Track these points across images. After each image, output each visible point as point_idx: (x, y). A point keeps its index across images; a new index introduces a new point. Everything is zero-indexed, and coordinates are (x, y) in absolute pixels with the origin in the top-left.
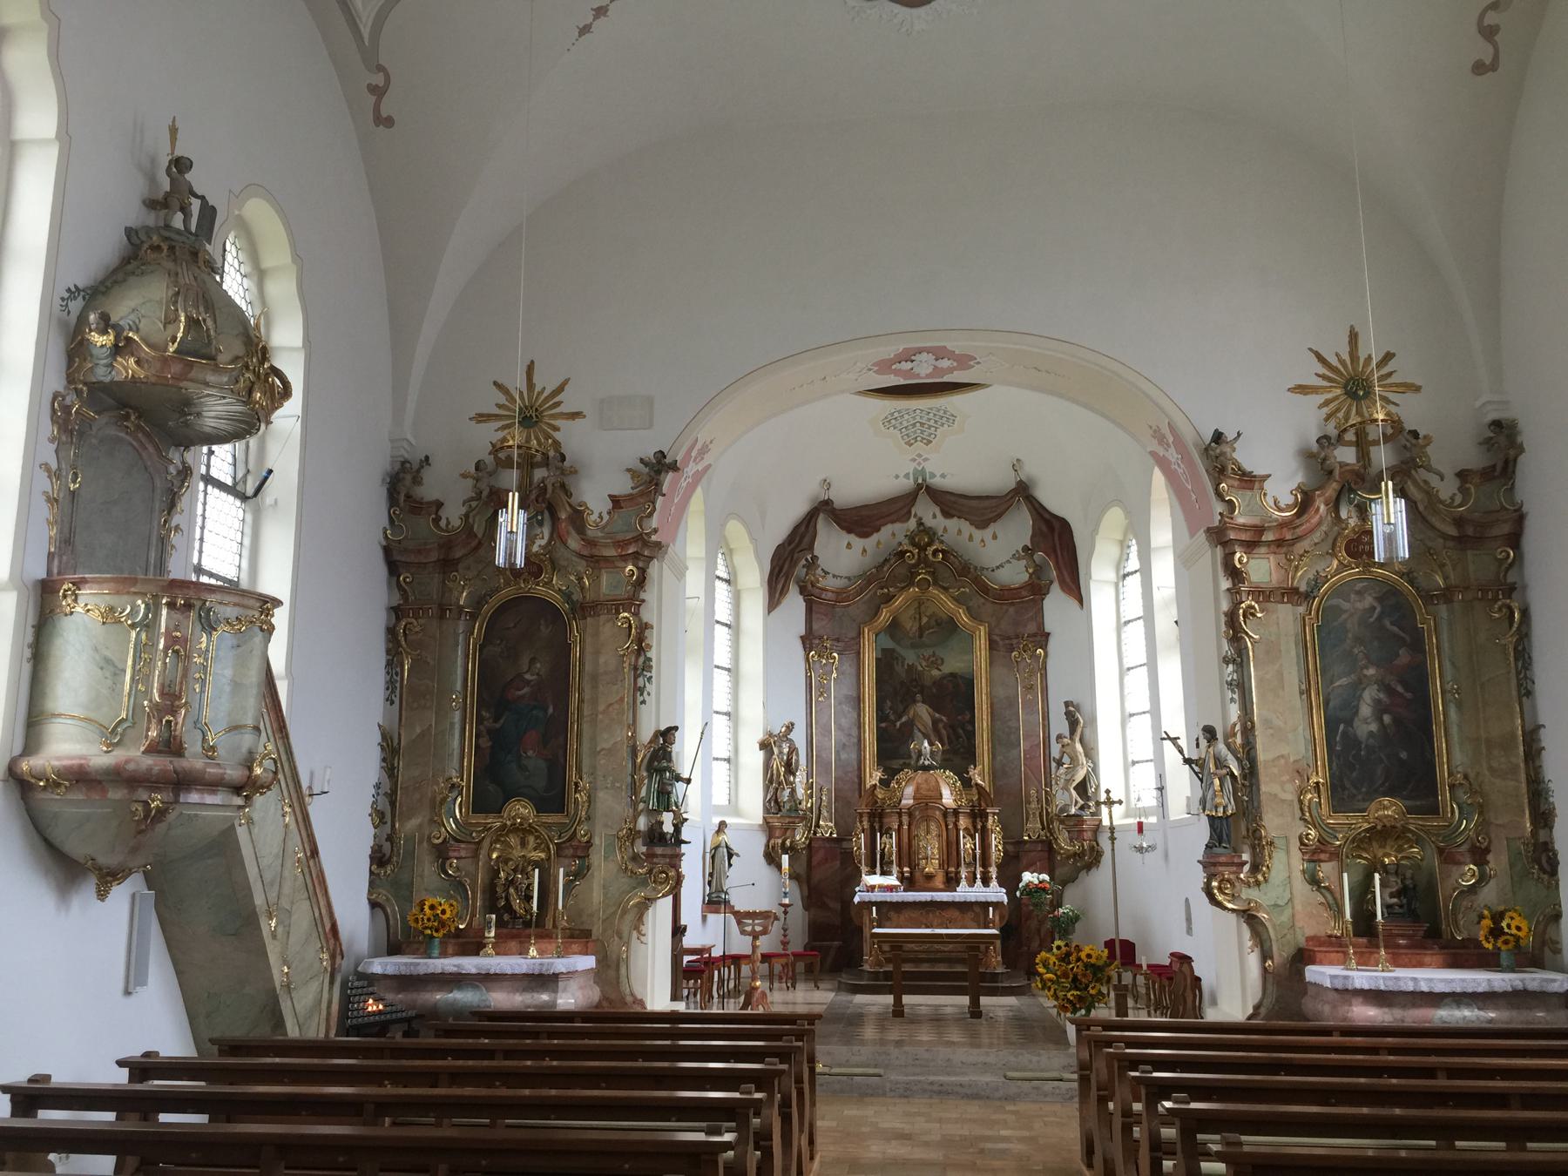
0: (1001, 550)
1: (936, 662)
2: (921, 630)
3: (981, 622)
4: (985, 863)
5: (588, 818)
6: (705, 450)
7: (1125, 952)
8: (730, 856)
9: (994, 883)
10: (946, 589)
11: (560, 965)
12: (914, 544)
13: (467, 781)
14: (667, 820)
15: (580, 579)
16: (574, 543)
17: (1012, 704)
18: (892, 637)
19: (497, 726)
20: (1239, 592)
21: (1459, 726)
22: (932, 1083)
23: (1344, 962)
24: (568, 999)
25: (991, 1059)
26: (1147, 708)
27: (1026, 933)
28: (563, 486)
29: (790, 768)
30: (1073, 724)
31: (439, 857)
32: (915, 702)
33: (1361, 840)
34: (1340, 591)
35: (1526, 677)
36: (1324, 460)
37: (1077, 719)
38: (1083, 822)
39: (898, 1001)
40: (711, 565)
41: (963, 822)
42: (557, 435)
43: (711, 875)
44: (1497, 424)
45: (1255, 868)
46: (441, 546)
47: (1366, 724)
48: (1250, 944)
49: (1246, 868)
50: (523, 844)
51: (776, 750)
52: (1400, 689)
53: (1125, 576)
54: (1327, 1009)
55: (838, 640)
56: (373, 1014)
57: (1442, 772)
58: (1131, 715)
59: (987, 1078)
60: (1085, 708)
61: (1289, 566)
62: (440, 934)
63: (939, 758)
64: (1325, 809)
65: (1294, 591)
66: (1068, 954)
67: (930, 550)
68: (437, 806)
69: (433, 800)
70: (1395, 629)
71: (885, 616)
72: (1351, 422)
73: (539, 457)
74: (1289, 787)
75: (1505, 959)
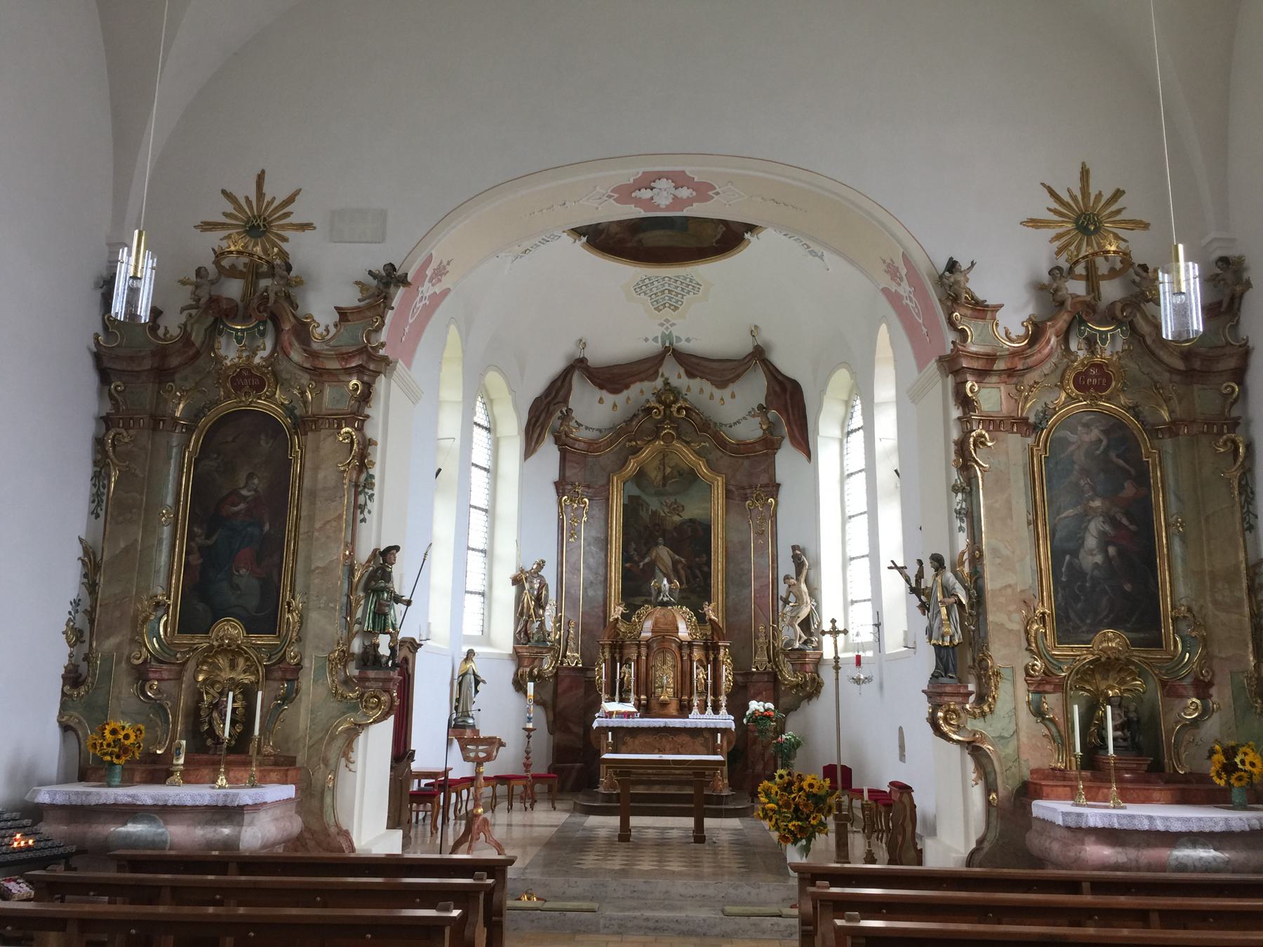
0: (738, 409)
1: (678, 509)
4: (716, 693)
5: (299, 640)
6: (440, 272)
7: (840, 776)
8: (477, 682)
9: (723, 711)
10: (688, 443)
11: (246, 796)
12: (660, 402)
13: (174, 600)
14: (384, 643)
15: (303, 393)
16: (296, 355)
17: (745, 546)
18: (638, 486)
19: (210, 542)
20: (969, 421)
21: (1184, 560)
22: (647, 919)
23: (1073, 796)
24: (256, 835)
25: (711, 891)
26: (867, 552)
27: (752, 759)
28: (288, 297)
29: (540, 602)
30: (799, 565)
31: (138, 679)
32: (657, 544)
33: (1085, 672)
34: (1065, 423)
35: (1248, 511)
36: (1056, 290)
38: (806, 655)
39: (625, 824)
40: (469, 411)
41: (697, 654)
42: (285, 246)
43: (458, 700)
44: (1224, 261)
45: (981, 699)
46: (153, 354)
47: (1091, 556)
48: (974, 776)
49: (972, 698)
50: (233, 666)
51: (527, 586)
52: (1125, 521)
53: (849, 433)
54: (1056, 847)
55: (588, 487)
56: (20, 850)
57: (1166, 604)
59: (704, 914)
60: (811, 553)
61: (1018, 396)
62: (122, 761)
63: (676, 594)
64: (1050, 640)
65: (1023, 421)
66: (790, 783)
67: (674, 408)
68: (138, 624)
69: (135, 617)
70: (1121, 462)
71: (632, 465)
72: (1083, 254)
73: (265, 268)
74: (1016, 617)
75: (1236, 796)
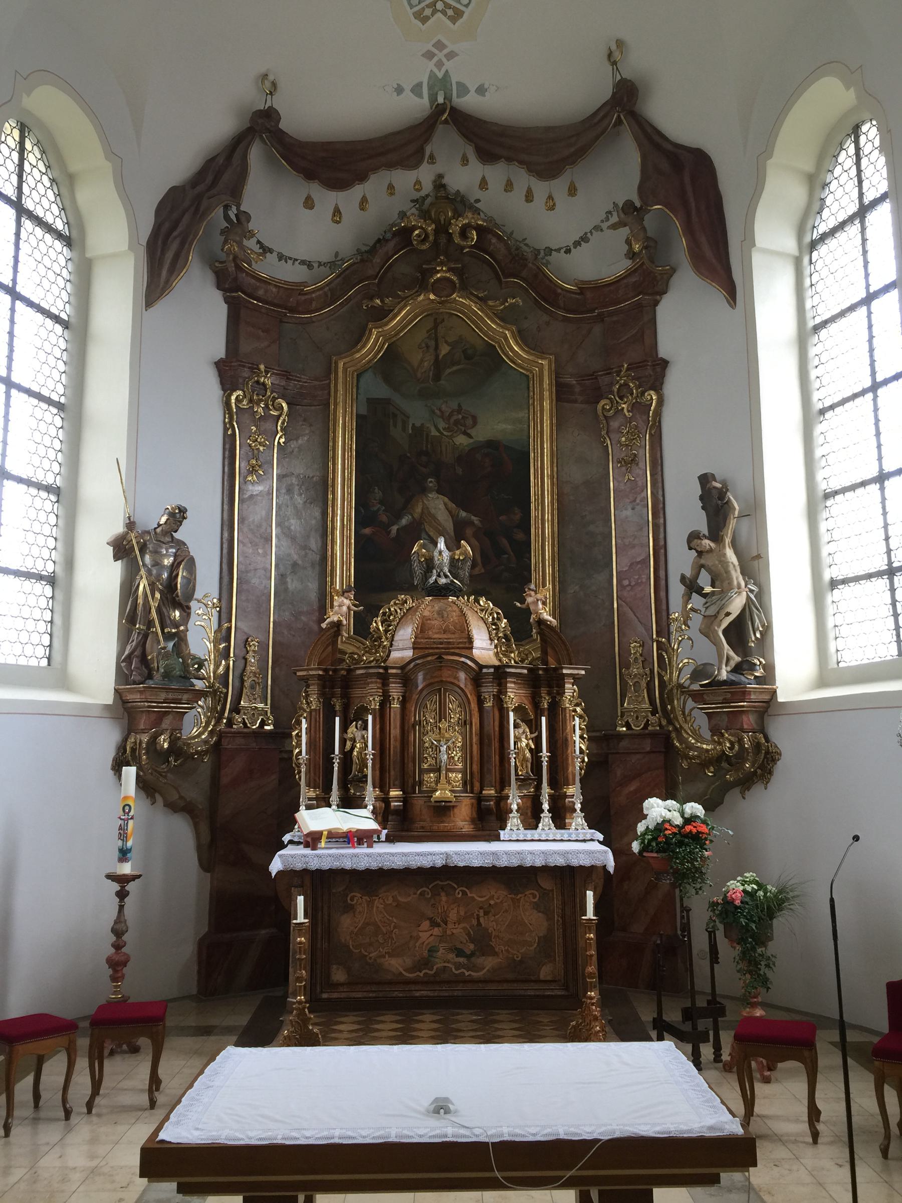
0: (575, 227)
1: (463, 422)
2: (438, 366)
3: (542, 353)
9: (578, 821)
18: (387, 379)
29: (175, 596)
32: (424, 490)
37: (724, 507)
38: (743, 694)
41: (514, 695)
53: (813, 245)
58: (827, 496)
63: (465, 572)
71: (373, 344)
